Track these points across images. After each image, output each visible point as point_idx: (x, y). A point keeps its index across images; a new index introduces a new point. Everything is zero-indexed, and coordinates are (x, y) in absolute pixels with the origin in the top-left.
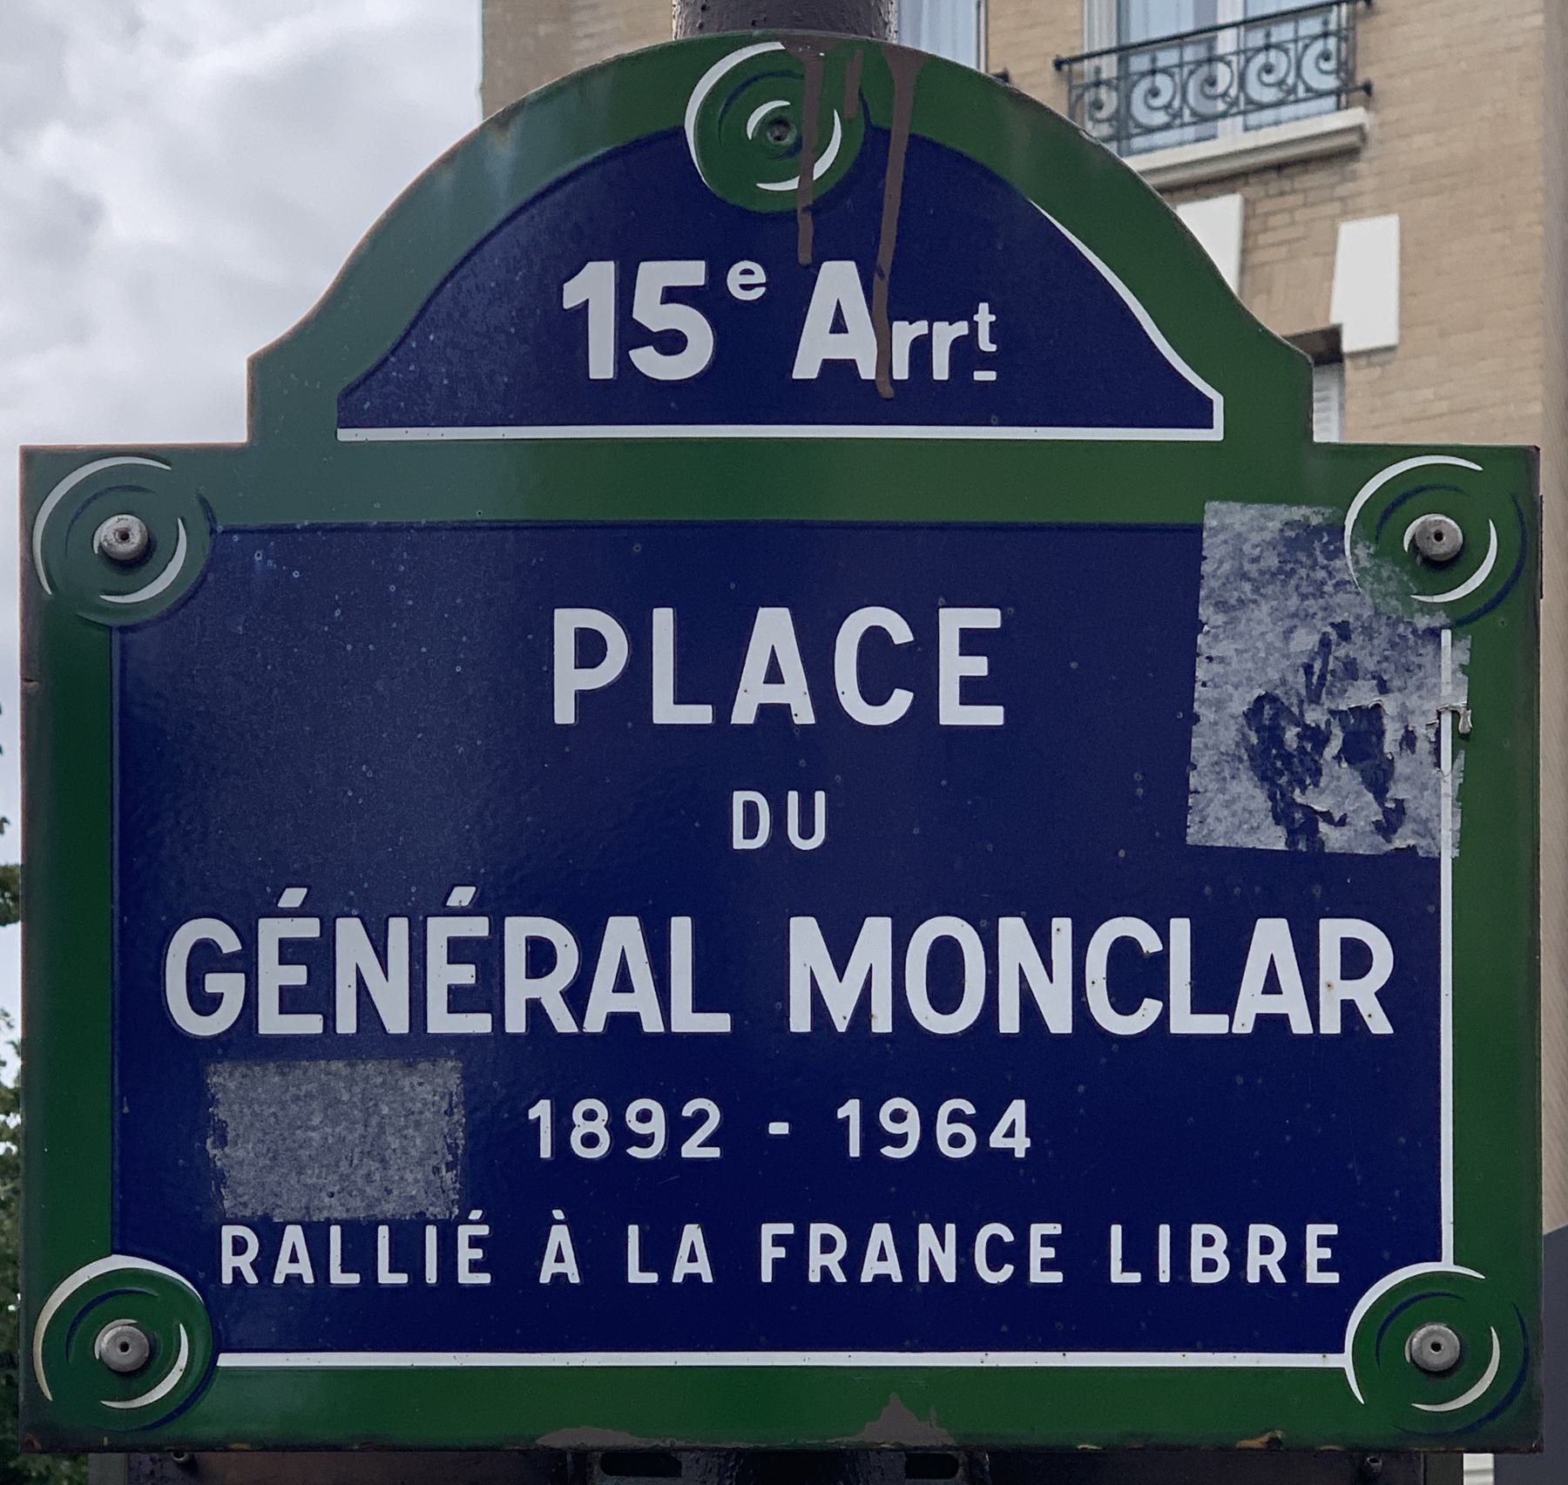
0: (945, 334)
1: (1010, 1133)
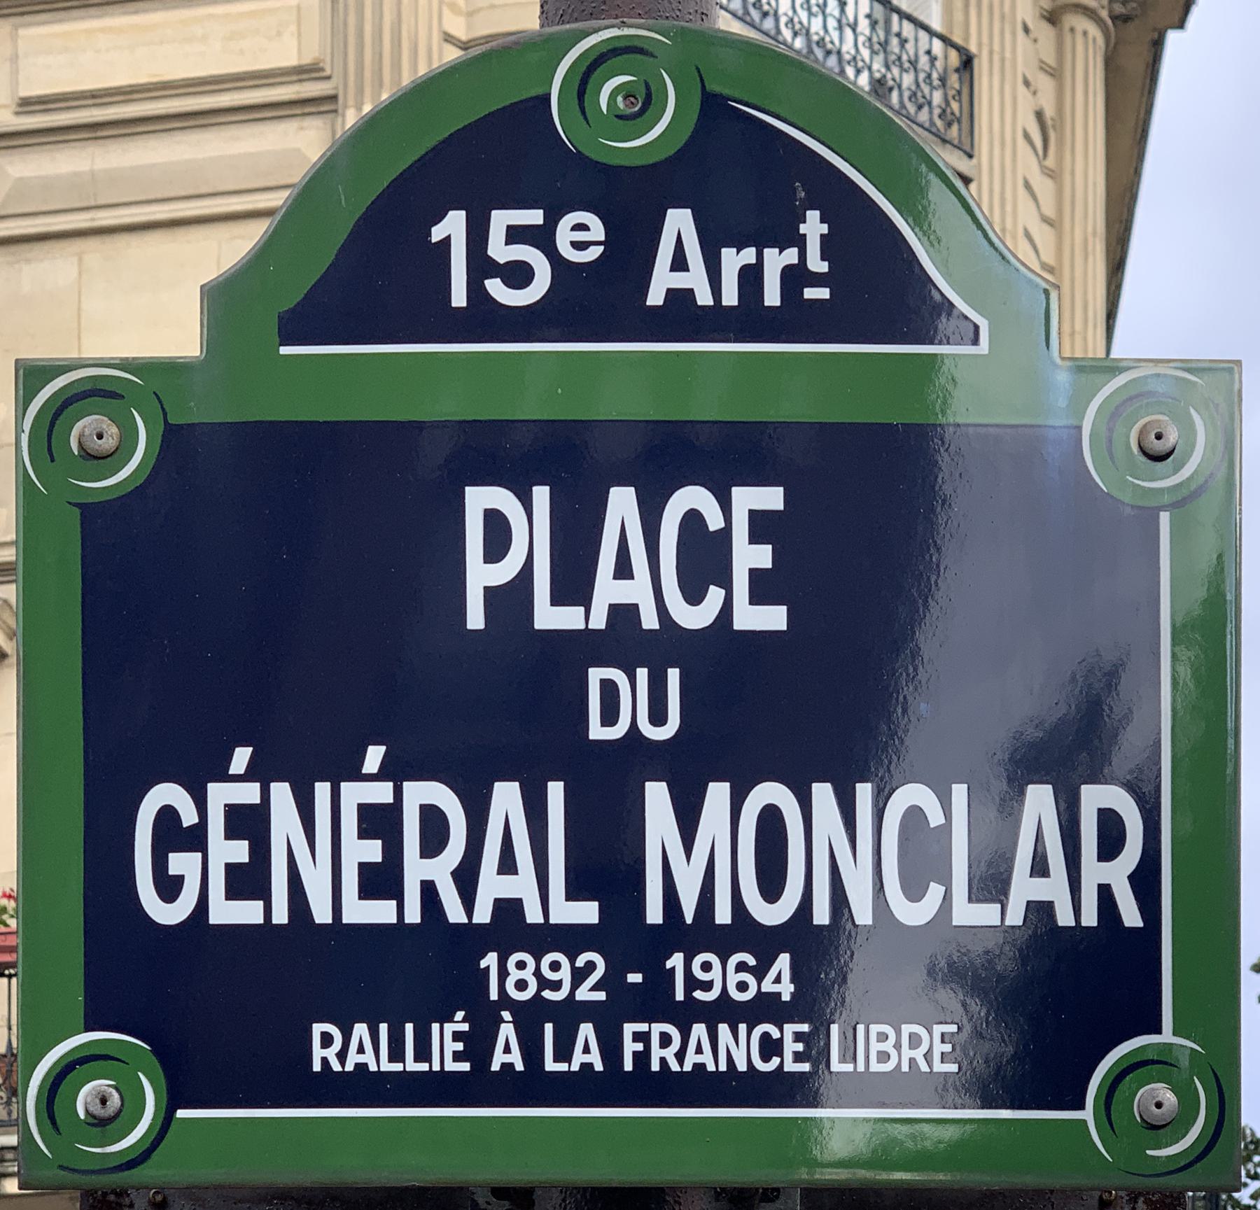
0: (776, 261)
1: (778, 980)
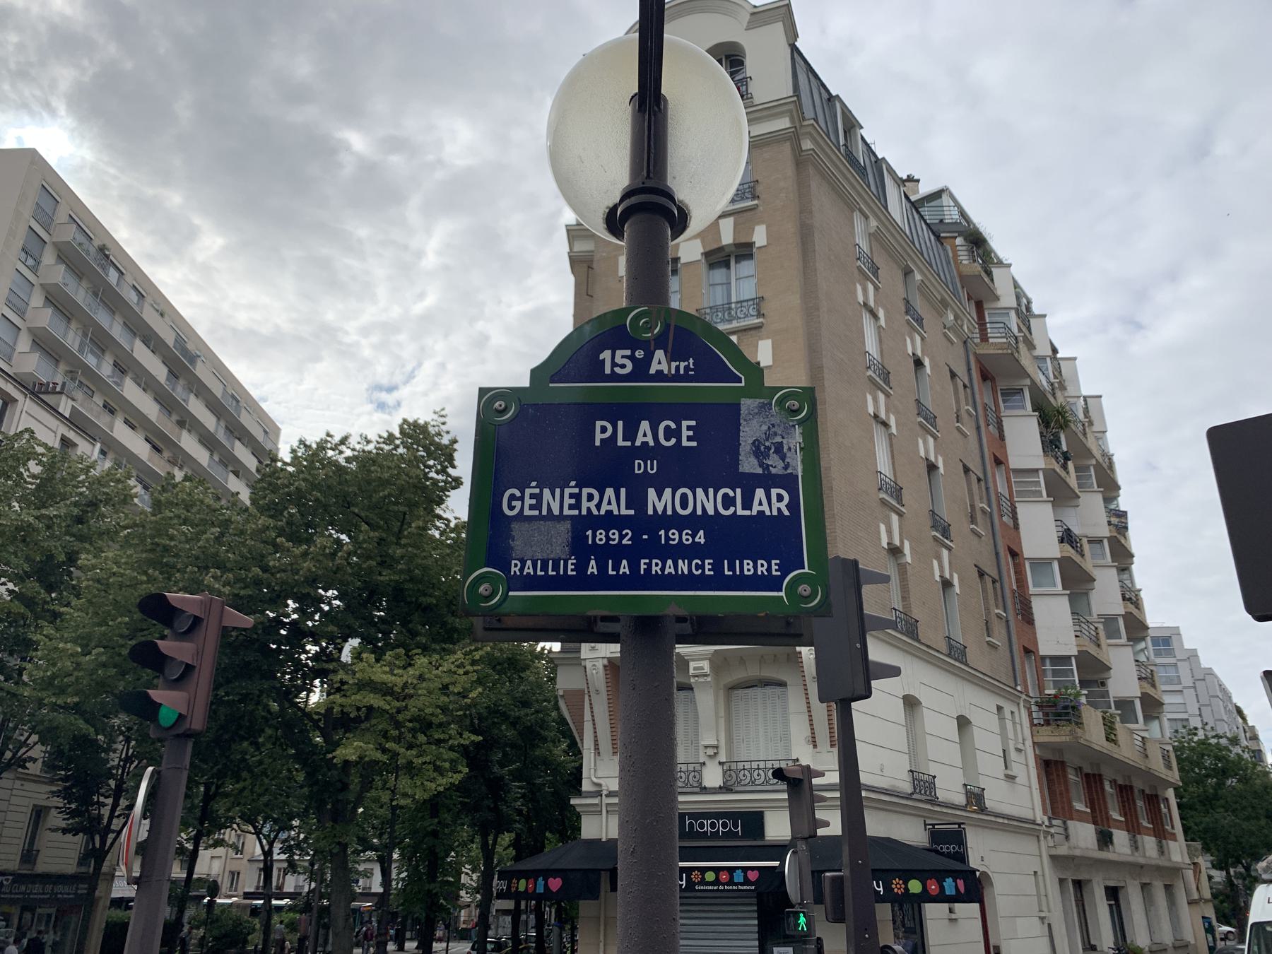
0: (683, 365)
